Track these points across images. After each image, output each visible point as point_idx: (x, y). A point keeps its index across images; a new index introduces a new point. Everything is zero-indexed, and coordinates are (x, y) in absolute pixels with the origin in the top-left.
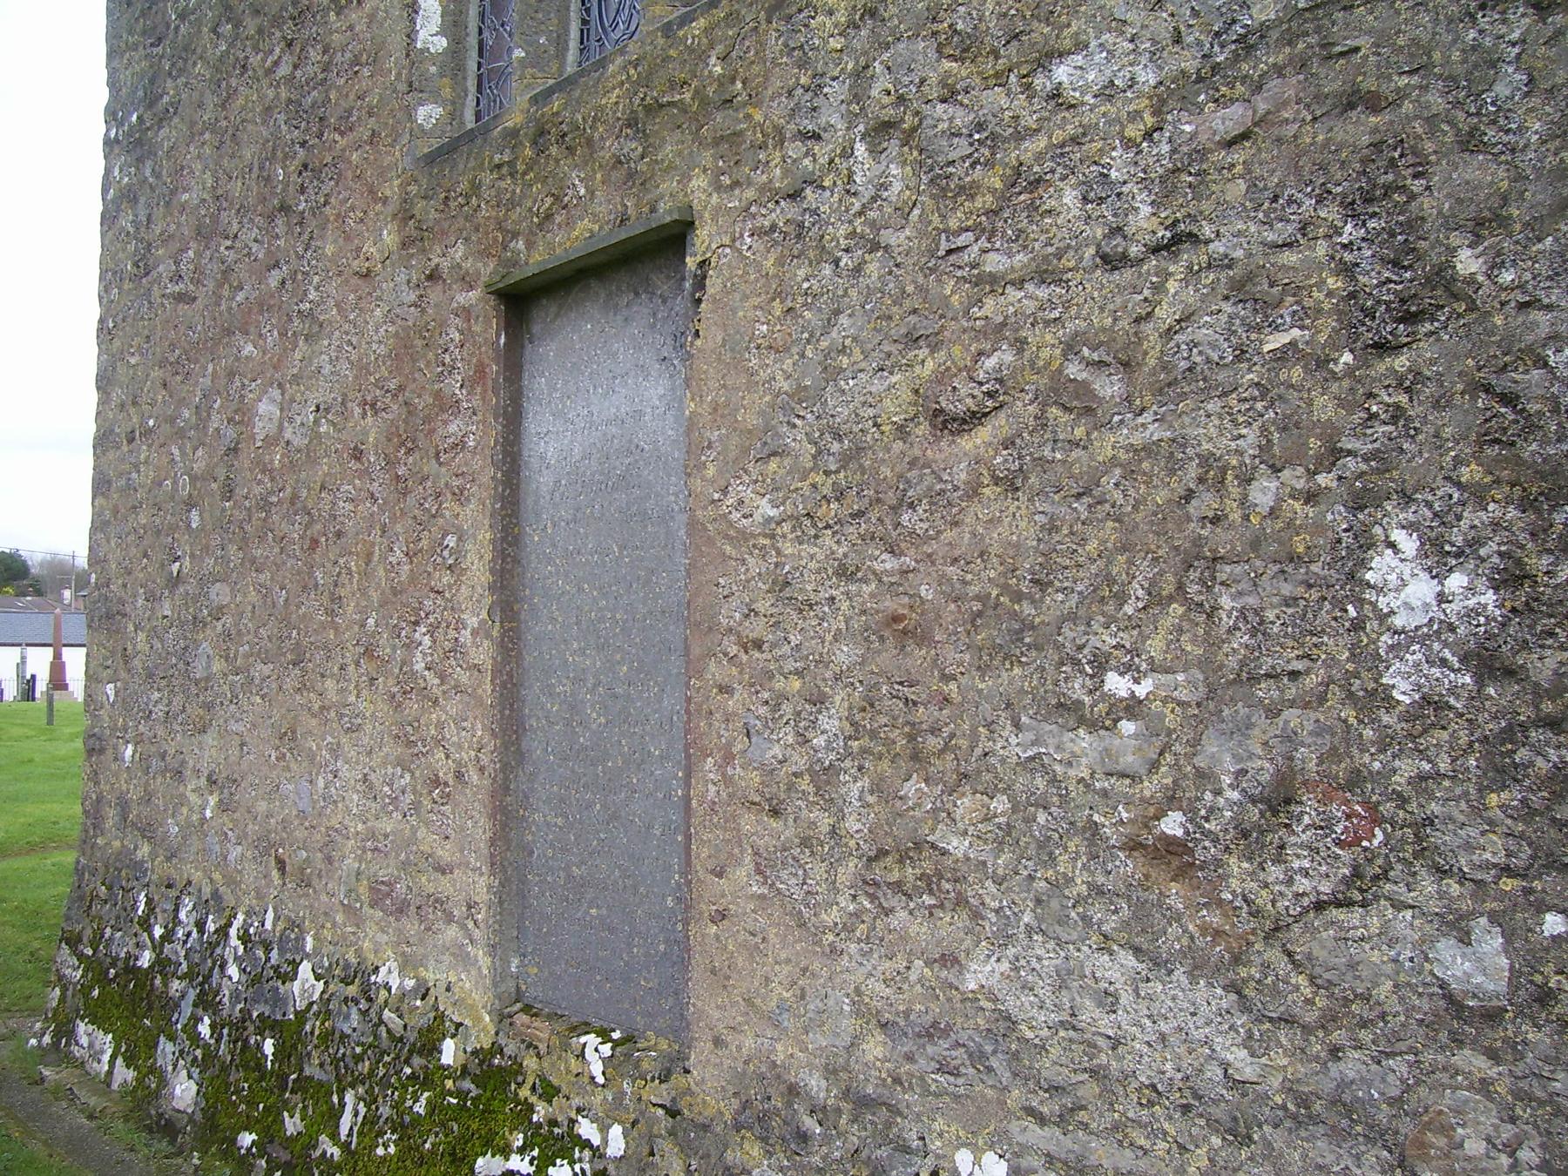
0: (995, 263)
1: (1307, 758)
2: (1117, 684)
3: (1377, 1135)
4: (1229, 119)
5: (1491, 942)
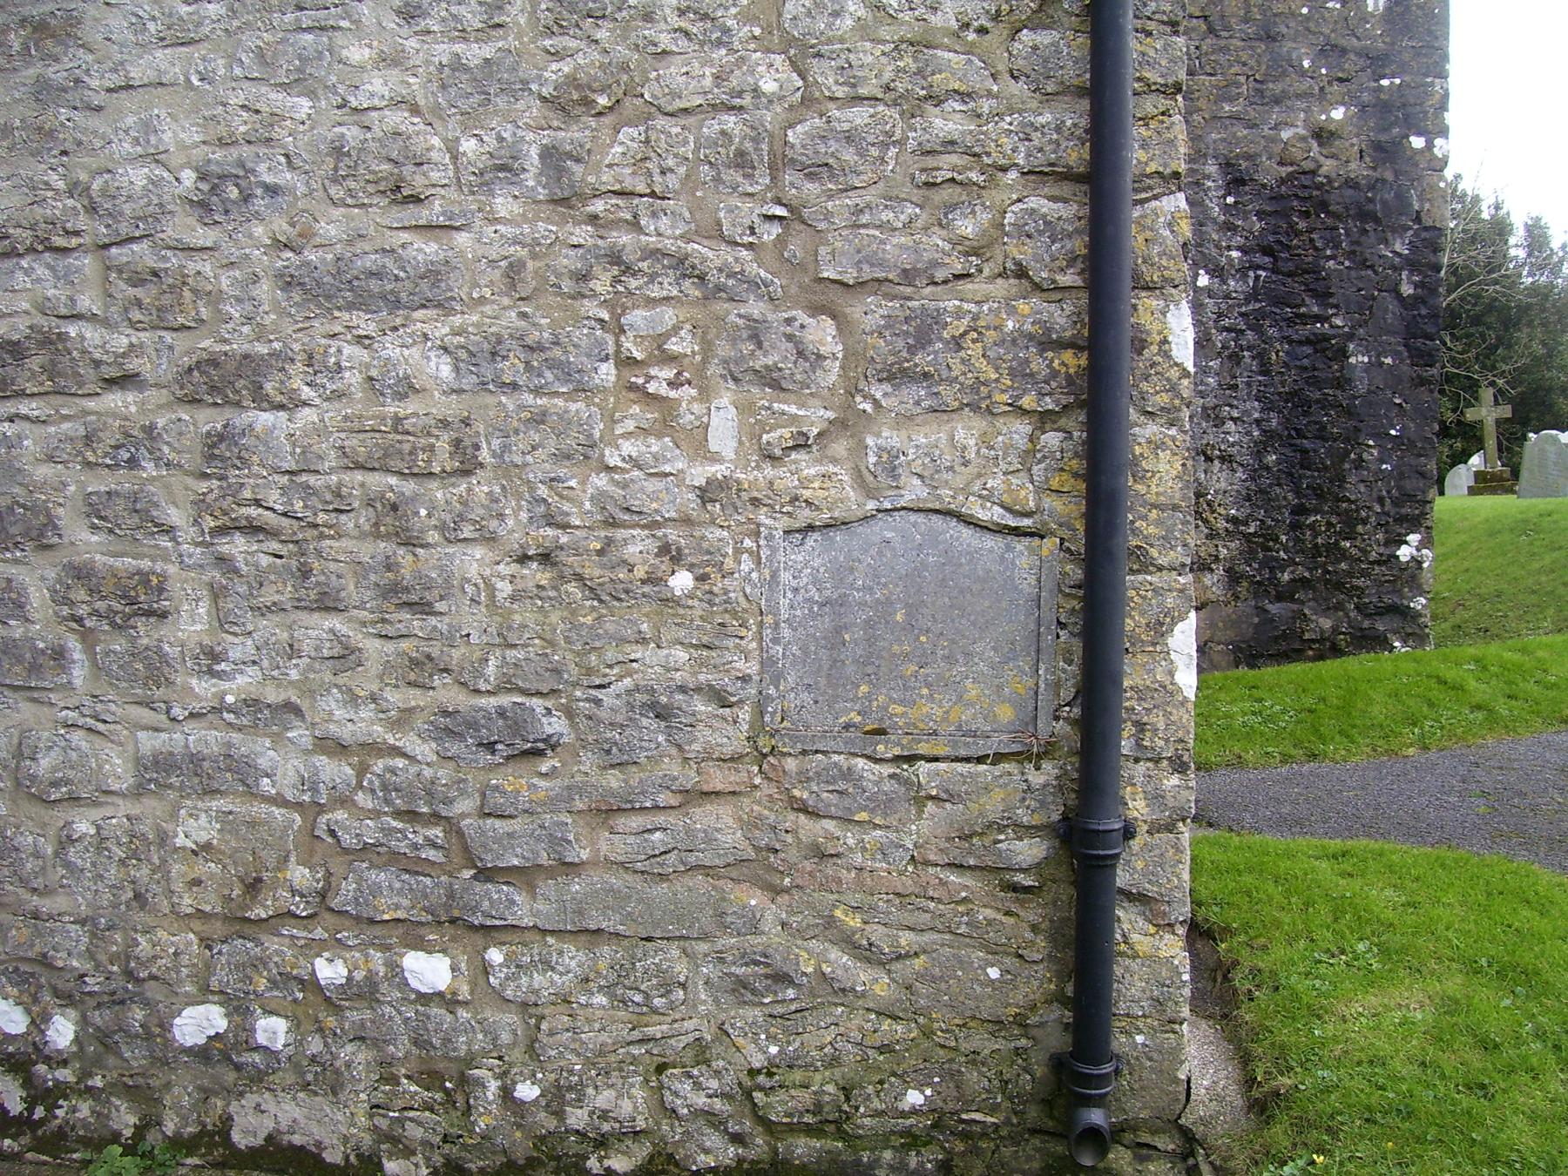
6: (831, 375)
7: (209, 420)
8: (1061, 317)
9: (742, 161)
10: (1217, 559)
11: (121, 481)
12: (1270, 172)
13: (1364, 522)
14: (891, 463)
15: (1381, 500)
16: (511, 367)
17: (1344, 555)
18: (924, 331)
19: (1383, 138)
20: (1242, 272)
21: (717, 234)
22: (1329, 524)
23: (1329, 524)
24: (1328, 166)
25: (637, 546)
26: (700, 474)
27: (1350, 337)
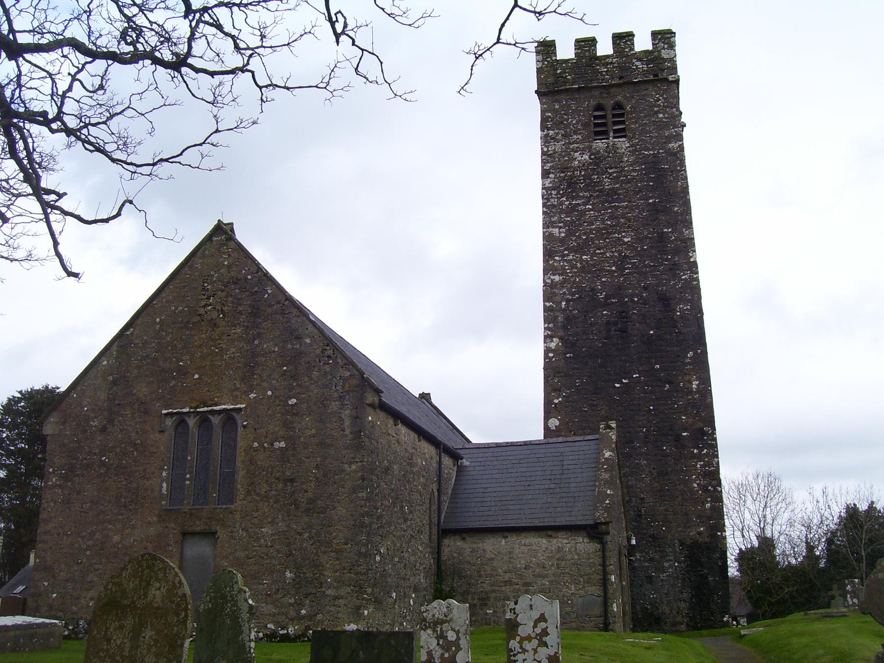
0: (255, 545)
1: (280, 587)
2: (265, 581)
3: (285, 614)
4: (277, 537)
5: (293, 599)
6: (582, 583)
7: (526, 588)
8: (602, 577)
9: (574, 564)
10: (684, 622)
11: (517, 594)
12: (689, 542)
13: (715, 613)
14: (588, 591)
15: (719, 608)
16: (554, 583)
17: (712, 620)
18: (590, 579)
19: (712, 533)
20: (684, 562)
21: (571, 571)
22: (708, 614)
23: (708, 614)
24: (701, 539)
25: (565, 599)
26: (571, 592)
27: (708, 574)
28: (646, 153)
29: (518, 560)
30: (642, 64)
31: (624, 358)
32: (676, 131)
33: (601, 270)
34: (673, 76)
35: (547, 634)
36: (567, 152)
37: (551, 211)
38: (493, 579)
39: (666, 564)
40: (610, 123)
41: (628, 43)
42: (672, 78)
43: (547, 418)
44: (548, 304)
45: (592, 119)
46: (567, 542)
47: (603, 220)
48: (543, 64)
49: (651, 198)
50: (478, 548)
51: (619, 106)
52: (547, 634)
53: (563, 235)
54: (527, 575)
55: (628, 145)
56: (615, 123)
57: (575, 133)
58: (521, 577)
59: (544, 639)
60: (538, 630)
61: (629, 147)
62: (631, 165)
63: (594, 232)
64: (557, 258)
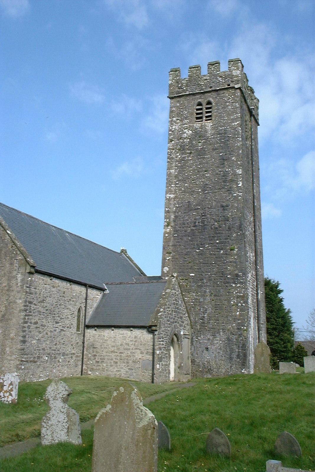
28: (221, 128)
29: (118, 341)
30: (222, 79)
31: (201, 237)
32: (237, 116)
33: (194, 191)
34: (238, 85)
35: (12, 391)
36: (181, 130)
37: (172, 161)
38: (107, 349)
39: (216, 342)
40: (204, 113)
41: (216, 67)
42: (237, 86)
43: (163, 267)
44: (167, 209)
45: (195, 111)
46: (139, 333)
47: (196, 165)
48: (172, 82)
49: (221, 153)
50: (102, 335)
51: (209, 103)
52: (12, 391)
53: (176, 173)
54: (121, 349)
55: (212, 124)
56: (207, 112)
57: (186, 119)
58: (118, 349)
59: (11, 392)
60: (9, 389)
61: (212, 125)
62: (212, 135)
63: (192, 171)
64: (172, 185)
